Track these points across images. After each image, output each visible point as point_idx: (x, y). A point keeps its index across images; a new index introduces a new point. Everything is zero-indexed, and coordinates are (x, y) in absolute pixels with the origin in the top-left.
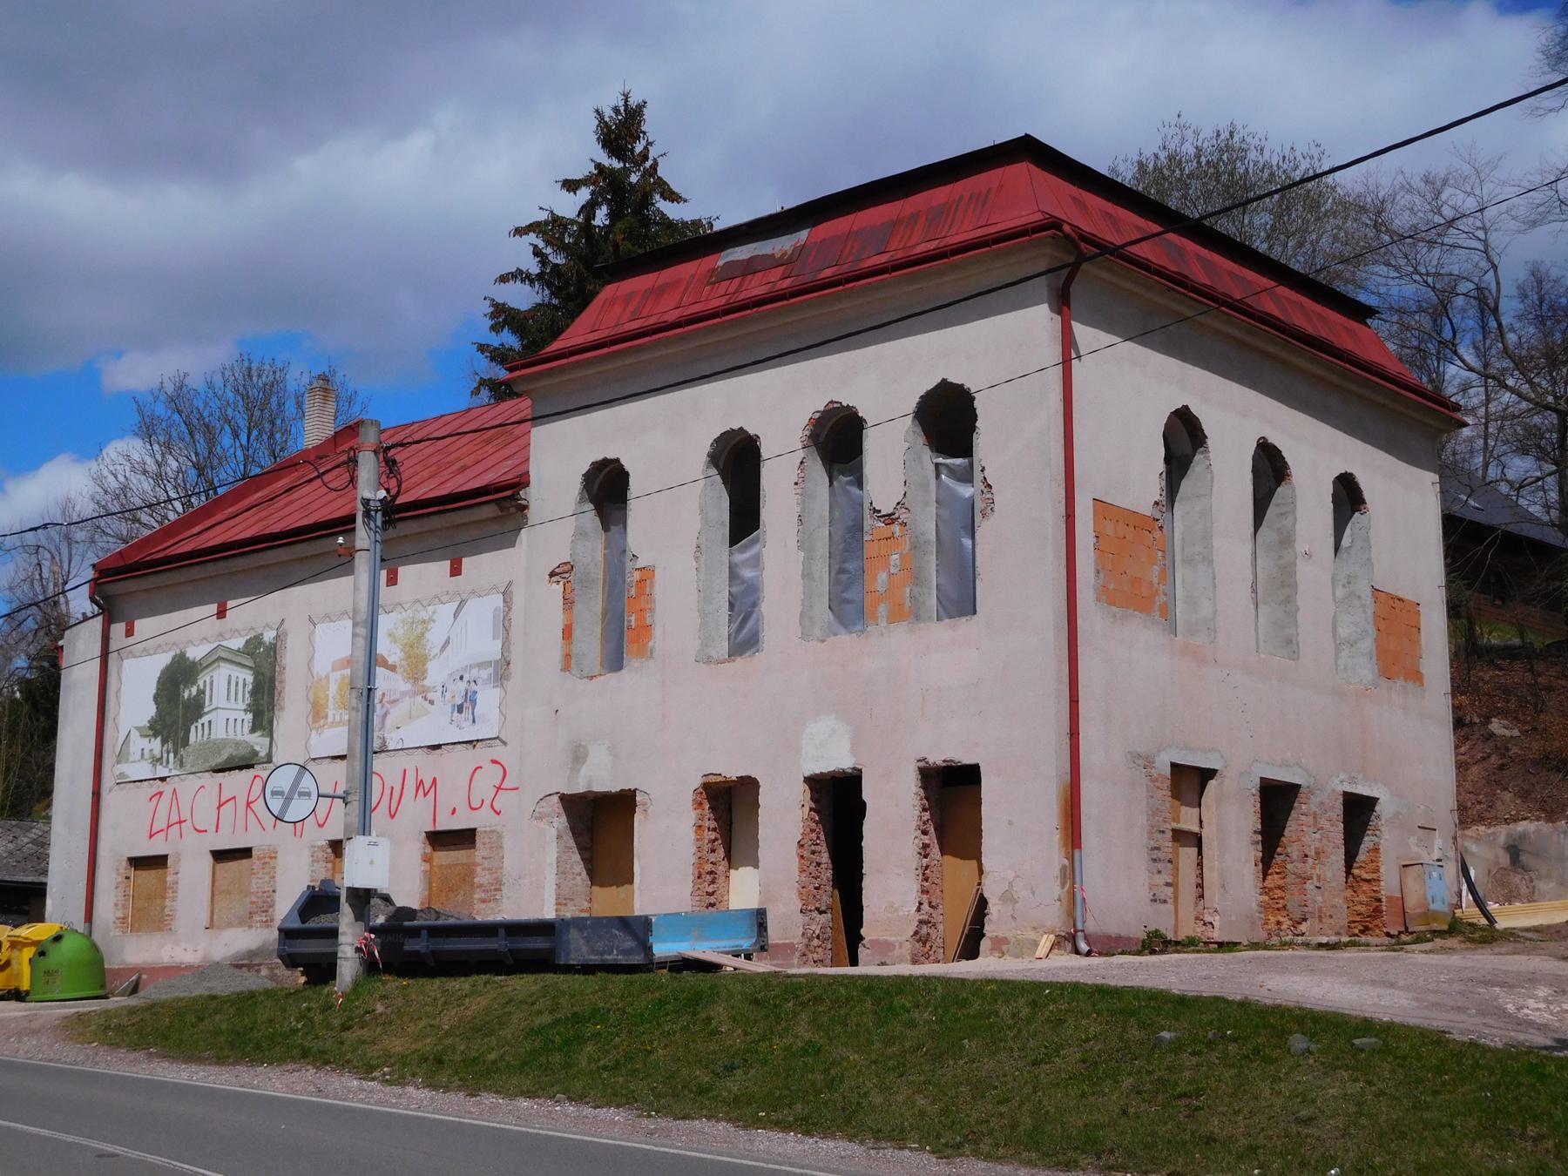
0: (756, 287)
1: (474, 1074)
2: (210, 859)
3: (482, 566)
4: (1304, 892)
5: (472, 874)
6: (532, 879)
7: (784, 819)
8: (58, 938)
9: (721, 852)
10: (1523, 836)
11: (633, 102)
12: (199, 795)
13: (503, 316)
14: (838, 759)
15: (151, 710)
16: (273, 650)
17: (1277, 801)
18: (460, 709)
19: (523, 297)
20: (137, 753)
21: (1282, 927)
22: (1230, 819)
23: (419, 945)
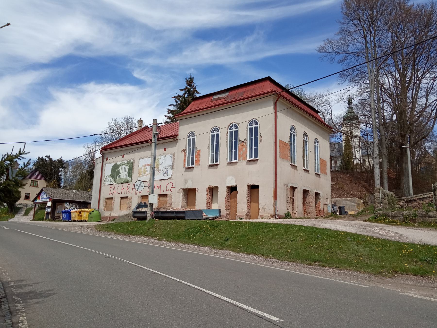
0: (219, 102)
1: (177, 239)
2: (120, 199)
3: (170, 150)
4: (309, 209)
5: (167, 202)
6: (177, 203)
7: (223, 193)
8: (93, 211)
9: (211, 199)
10: (337, 200)
11: (192, 77)
12: (119, 187)
13: (170, 111)
14: (233, 184)
15: (111, 173)
16: (132, 163)
17: (305, 192)
18: (165, 173)
19: (172, 108)
20: (108, 180)
21: (306, 215)
22: (299, 196)
23: (160, 215)
